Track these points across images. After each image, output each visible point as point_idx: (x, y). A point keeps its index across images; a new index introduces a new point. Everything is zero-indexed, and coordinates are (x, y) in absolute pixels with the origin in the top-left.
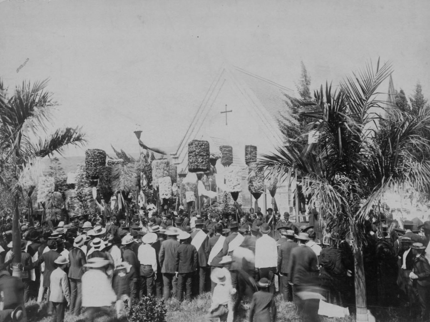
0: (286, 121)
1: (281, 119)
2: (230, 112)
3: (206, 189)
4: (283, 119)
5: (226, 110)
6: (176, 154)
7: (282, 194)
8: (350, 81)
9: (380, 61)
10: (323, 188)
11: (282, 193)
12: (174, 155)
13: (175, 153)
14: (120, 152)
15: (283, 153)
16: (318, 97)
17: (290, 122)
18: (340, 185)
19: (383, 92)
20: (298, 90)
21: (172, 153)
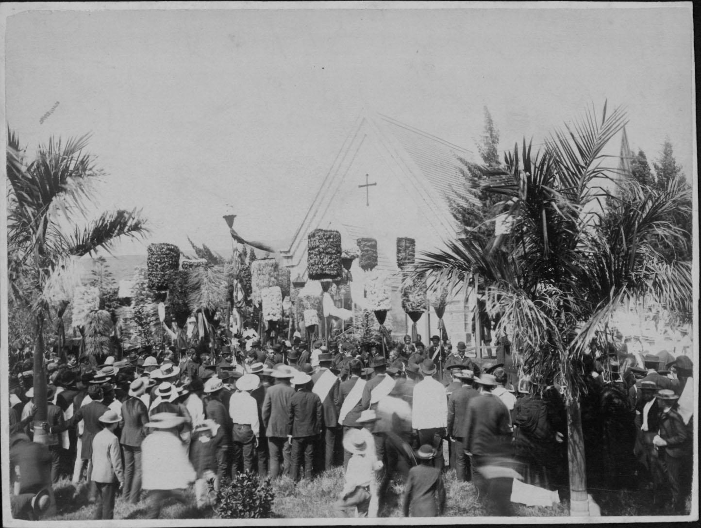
0: (461, 199)
1: (453, 196)
2: (374, 186)
8: (561, 138)
12: (286, 252)
13: (287, 250)
14: (202, 248)
15: (456, 249)
16: (511, 162)
18: (545, 300)
21: (282, 250)
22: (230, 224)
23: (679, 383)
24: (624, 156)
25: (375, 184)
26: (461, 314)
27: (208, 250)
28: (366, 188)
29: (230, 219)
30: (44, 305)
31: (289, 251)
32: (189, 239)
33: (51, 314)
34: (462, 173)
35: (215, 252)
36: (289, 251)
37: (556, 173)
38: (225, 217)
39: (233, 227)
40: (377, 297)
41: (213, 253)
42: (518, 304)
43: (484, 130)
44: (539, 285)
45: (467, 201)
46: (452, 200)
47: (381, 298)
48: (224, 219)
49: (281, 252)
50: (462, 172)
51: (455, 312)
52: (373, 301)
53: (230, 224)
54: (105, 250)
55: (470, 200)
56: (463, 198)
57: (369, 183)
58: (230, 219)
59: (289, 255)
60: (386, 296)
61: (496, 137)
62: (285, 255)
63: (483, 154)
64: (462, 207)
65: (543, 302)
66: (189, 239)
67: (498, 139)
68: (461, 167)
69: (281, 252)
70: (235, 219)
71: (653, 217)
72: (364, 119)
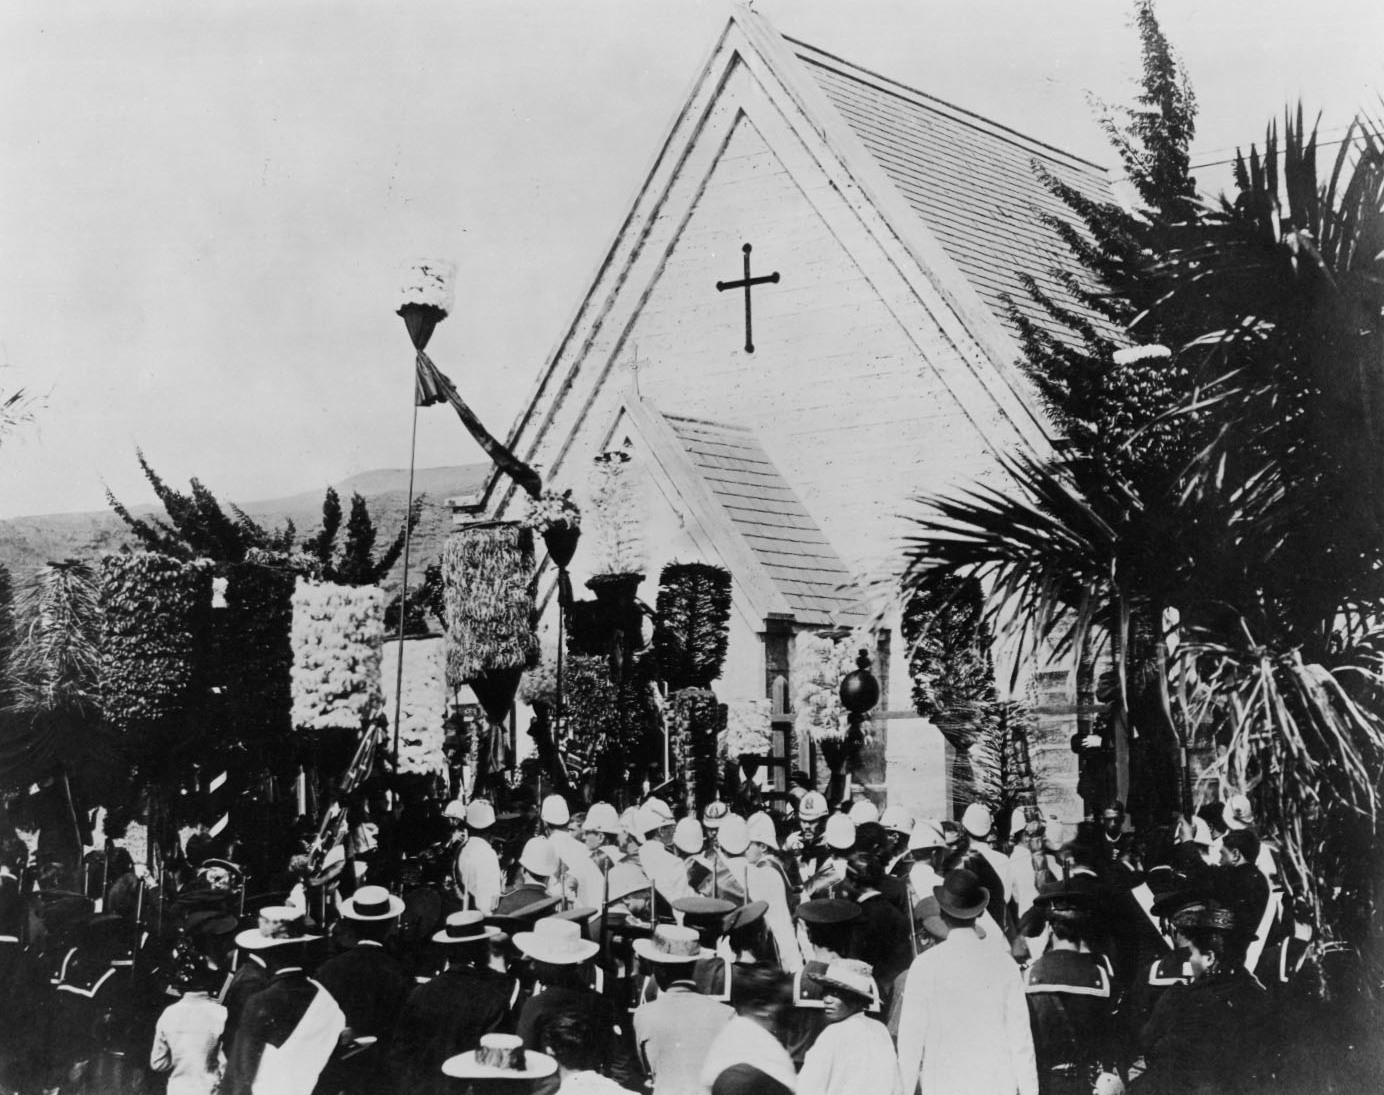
12: (473, 510)
14: (187, 492)
21: (460, 502)
22: (421, 337)
24: (653, 447)
26: (1066, 717)
27: (211, 500)
28: (742, 290)
29: (422, 320)
30: (874, 840)
31: (480, 508)
32: (144, 463)
35: (234, 507)
36: (480, 508)
38: (407, 311)
39: (425, 351)
40: (325, 681)
41: (226, 511)
43: (1144, 91)
44: (1339, 622)
45: (1088, 333)
47: (335, 687)
48: (401, 320)
49: (456, 510)
52: (309, 692)
53: (421, 337)
55: (1100, 333)
56: (1075, 322)
58: (422, 320)
59: (483, 518)
60: (356, 678)
61: (1185, 117)
62: (468, 518)
63: (1138, 174)
64: (1071, 354)
65: (1366, 672)
66: (144, 463)
67: (1191, 126)
68: (1066, 220)
69: (456, 510)
70: (439, 327)
72: (736, 58)
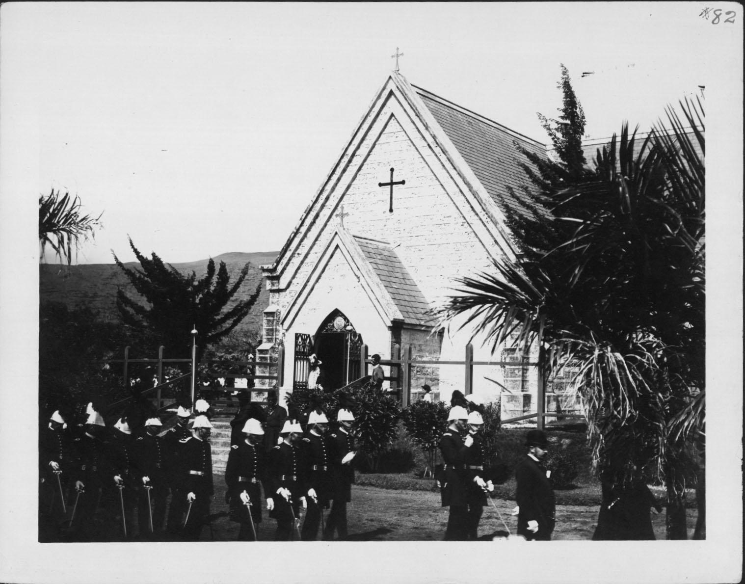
0: (525, 209)
1: (513, 204)
2: (401, 185)
3: (360, 335)
4: (517, 204)
5: (392, 180)
6: (275, 269)
7: (507, 367)
8: (678, 131)
9: (459, 327)
10: (601, 357)
11: (509, 364)
12: (268, 270)
13: (271, 267)
14: (150, 258)
15: (513, 277)
16: (606, 158)
17: (535, 212)
18: (643, 355)
19: (667, 116)
20: (555, 145)
21: (266, 267)
23: (534, 532)
25: (403, 182)
33: (253, 273)
34: (528, 173)
37: (668, 179)
42: (601, 357)
46: (512, 209)
50: (527, 170)
51: (509, 364)
54: (662, 122)
56: (528, 207)
57: (394, 181)
62: (269, 274)
71: (238, 346)
